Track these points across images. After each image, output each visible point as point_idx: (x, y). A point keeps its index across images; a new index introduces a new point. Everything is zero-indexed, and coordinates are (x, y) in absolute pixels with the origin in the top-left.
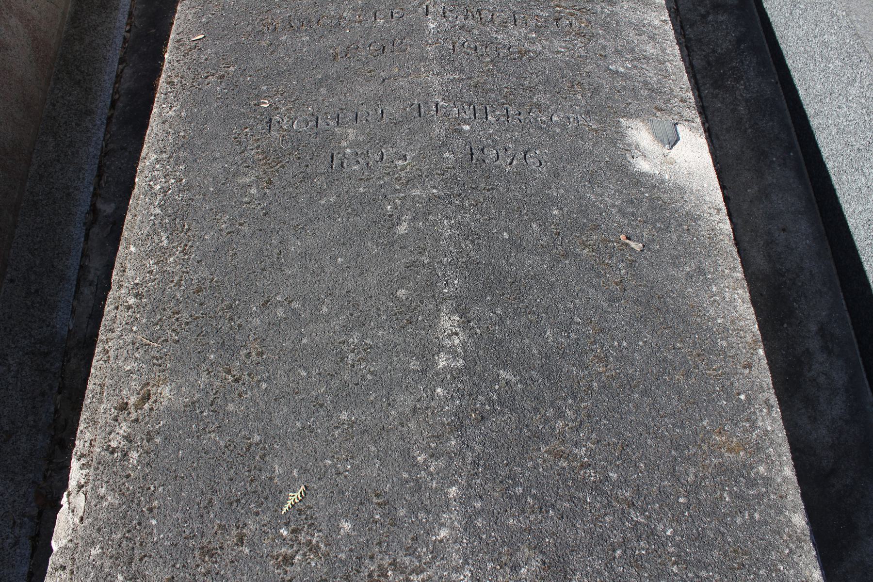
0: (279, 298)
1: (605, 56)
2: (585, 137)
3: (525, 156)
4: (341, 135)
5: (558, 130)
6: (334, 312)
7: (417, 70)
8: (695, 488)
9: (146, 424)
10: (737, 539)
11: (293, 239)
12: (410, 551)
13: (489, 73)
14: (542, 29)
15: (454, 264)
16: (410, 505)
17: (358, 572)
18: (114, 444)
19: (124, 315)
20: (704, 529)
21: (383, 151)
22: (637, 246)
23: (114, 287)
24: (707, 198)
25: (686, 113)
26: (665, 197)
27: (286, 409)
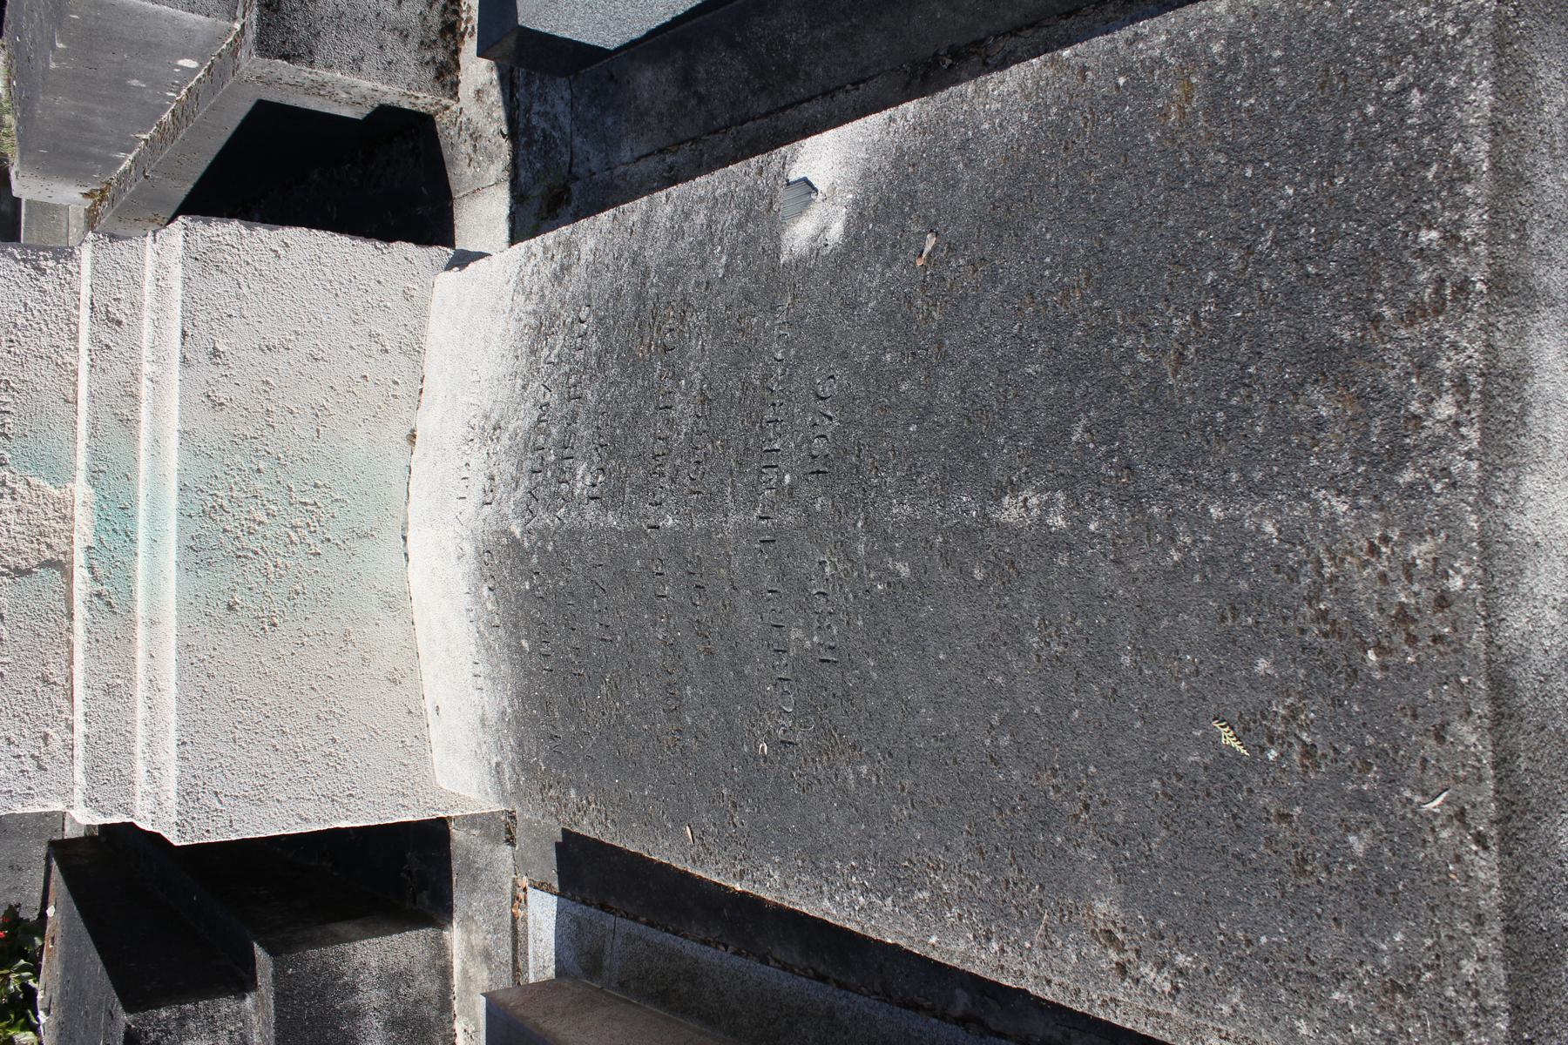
0: (988, 742)
2: (802, 314)
5: (793, 352)
6: (1003, 668)
7: (721, 543)
8: (1233, 150)
9: (1142, 938)
10: (1307, 84)
11: (919, 719)
12: (1294, 575)
15: (944, 500)
16: (1233, 574)
17: (1321, 651)
18: (1167, 987)
19: (1012, 960)
20: (1289, 138)
22: (931, 242)
23: (1023, 984)
24: (876, 137)
25: (775, 168)
26: (874, 199)
27: (1120, 741)
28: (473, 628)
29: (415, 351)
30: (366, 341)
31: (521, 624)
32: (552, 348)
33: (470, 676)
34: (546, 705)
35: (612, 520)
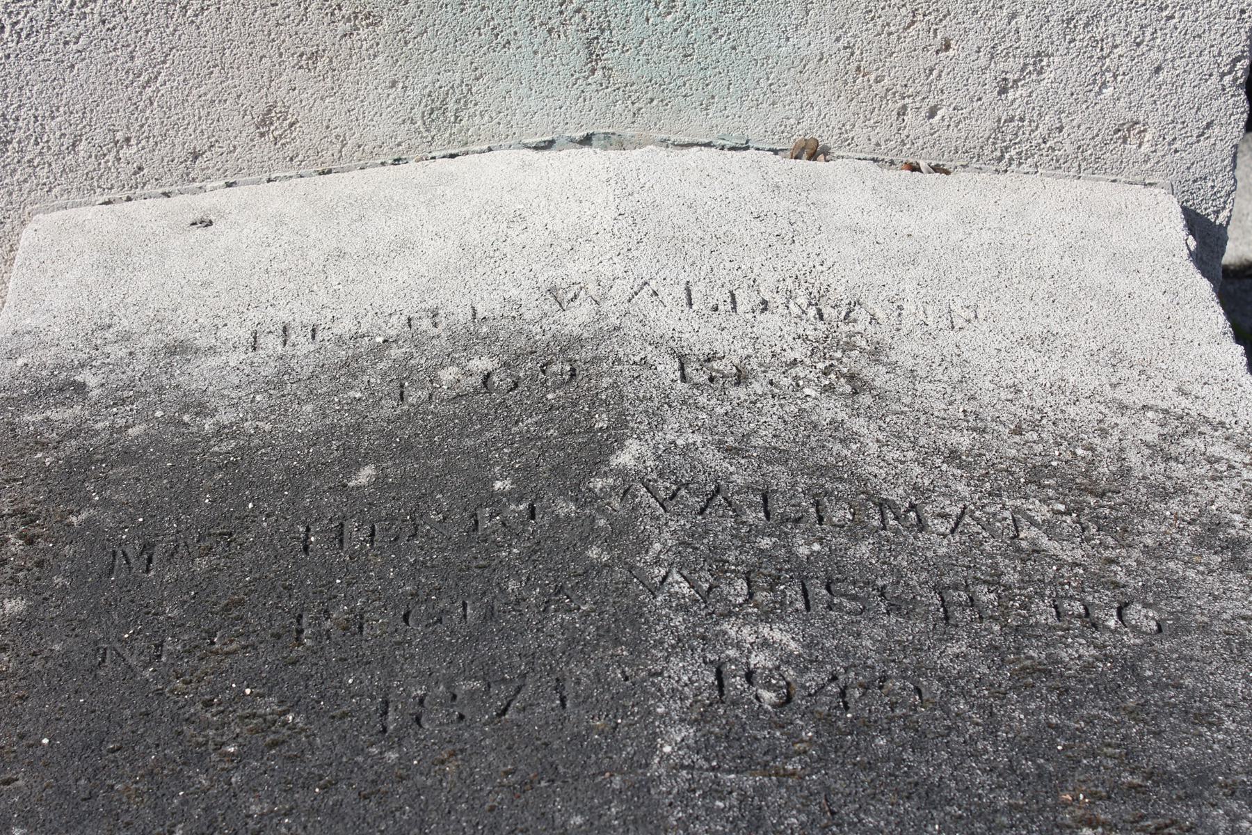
28: (395, 326)
29: (1003, 152)
30: (1028, 44)
31: (412, 466)
32: (1050, 529)
33: (284, 316)
34: (224, 534)
35: (675, 739)
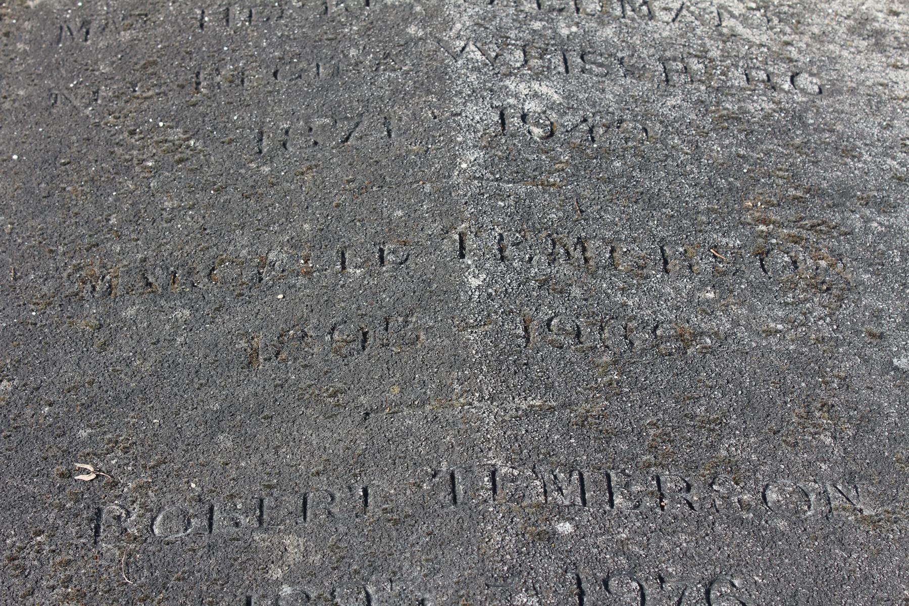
1: (881, 336)
2: (848, 538)
3: (708, 592)
4: (269, 550)
5: (782, 524)
13: (612, 391)
14: (729, 279)
21: (371, 589)
32: (744, 20)
